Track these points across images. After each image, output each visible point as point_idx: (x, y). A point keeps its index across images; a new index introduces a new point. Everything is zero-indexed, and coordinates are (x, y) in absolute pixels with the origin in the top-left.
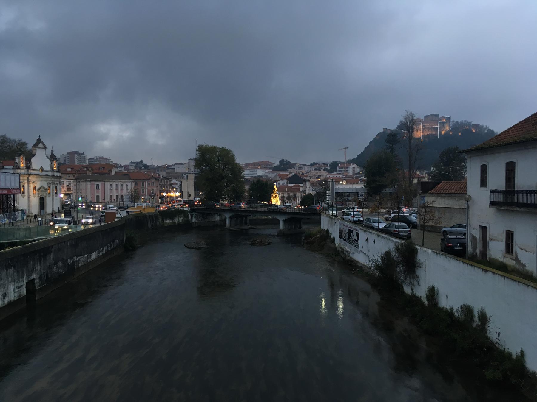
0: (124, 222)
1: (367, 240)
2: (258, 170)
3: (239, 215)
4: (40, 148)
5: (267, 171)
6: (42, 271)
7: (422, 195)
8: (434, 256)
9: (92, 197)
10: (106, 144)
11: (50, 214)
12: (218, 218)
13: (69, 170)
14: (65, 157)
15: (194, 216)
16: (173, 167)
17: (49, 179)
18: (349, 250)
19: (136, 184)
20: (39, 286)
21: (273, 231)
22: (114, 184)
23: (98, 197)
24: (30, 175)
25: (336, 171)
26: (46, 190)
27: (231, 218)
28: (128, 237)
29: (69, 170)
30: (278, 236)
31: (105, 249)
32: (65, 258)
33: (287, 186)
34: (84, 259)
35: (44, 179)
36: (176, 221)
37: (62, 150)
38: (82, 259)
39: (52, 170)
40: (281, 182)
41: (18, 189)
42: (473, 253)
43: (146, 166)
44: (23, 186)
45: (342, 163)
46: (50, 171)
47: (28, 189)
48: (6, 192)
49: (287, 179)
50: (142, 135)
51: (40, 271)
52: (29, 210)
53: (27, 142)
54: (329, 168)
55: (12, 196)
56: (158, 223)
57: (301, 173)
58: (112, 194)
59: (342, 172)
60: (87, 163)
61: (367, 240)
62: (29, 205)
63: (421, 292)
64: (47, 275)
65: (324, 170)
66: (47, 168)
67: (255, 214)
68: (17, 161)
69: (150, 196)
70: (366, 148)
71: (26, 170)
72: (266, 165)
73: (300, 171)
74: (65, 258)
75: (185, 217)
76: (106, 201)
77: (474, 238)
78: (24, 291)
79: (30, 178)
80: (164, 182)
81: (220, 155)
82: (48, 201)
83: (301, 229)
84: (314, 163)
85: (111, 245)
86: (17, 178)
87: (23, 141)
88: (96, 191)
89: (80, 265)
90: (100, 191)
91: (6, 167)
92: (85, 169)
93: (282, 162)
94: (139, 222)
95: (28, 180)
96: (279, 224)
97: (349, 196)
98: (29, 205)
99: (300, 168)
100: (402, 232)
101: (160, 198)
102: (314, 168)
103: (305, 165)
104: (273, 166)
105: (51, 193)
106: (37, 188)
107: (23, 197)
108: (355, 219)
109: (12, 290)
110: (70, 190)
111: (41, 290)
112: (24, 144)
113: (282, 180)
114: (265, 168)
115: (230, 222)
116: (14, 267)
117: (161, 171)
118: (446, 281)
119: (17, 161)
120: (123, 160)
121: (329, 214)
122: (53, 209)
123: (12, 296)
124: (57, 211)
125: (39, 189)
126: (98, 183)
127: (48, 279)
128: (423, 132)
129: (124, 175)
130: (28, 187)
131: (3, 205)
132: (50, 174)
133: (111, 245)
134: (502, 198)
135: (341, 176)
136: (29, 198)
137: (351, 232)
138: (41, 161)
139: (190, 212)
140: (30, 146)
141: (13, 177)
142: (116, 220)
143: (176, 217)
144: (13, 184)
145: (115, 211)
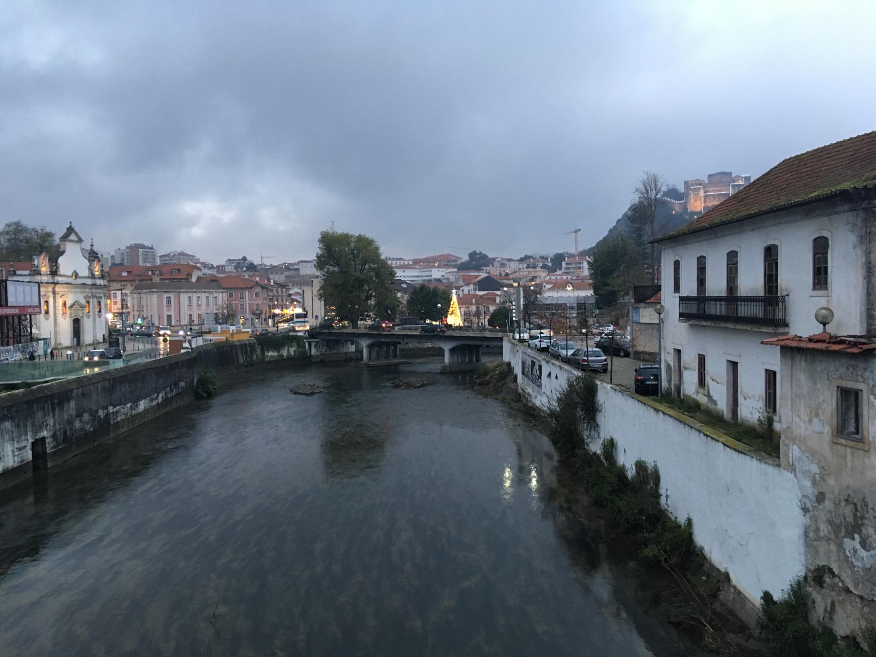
0: (193, 355)
1: (549, 375)
2: (433, 270)
3: (383, 343)
4: (71, 241)
5: (449, 270)
6: (58, 427)
7: (636, 305)
8: (612, 394)
9: (160, 318)
10: (197, 231)
11: (90, 345)
12: (352, 348)
13: (125, 274)
14: (123, 254)
15: (313, 345)
16: (296, 267)
17: (88, 290)
18: (531, 393)
19: (231, 295)
20: (53, 448)
21: (435, 366)
22: (194, 297)
23: (169, 317)
24: (56, 283)
25: (561, 269)
26: (82, 307)
27: (370, 347)
28: (208, 377)
29: (125, 274)
30: (441, 373)
31: (161, 395)
32: (94, 408)
33: (475, 296)
34: (125, 410)
35: (79, 290)
36: (284, 352)
37: (111, 242)
38: (122, 410)
39: (93, 276)
40: (466, 289)
41: (36, 307)
42: (668, 389)
43: (252, 267)
44: (47, 302)
45: (571, 256)
46: (88, 277)
47: (55, 306)
48: (17, 311)
49: (475, 284)
50: (247, 216)
51: (54, 425)
52: (56, 339)
53: (53, 232)
54: (550, 264)
55: (28, 317)
56: (255, 357)
57: (503, 274)
58: (191, 313)
59: (571, 270)
60: (158, 262)
61: (549, 375)
62: (56, 333)
63: (596, 447)
64: (65, 433)
65: (542, 267)
66: (84, 272)
67: (406, 341)
68: (36, 263)
69: (254, 314)
70: (611, 231)
71: (50, 277)
72: (446, 261)
73: (502, 269)
74: (94, 408)
75: (299, 346)
76: (182, 323)
77: (669, 367)
78: (28, 455)
79: (57, 289)
80: (277, 291)
81: (355, 248)
82: (87, 325)
83: (474, 365)
84: (526, 256)
85: (171, 390)
86: (36, 289)
87: (48, 230)
88: (165, 307)
89: (119, 419)
90: (173, 308)
91: (18, 272)
92: (150, 273)
93: (473, 255)
94: (223, 355)
95: (54, 293)
96: (444, 355)
97: (548, 309)
98: (56, 333)
99: (503, 265)
100: (594, 361)
101: (270, 317)
102: (525, 265)
103: (510, 260)
104: (459, 262)
105: (91, 313)
106: (68, 305)
107: (47, 319)
108: (544, 345)
109: (10, 454)
110: (127, 308)
111: (54, 454)
112: (50, 235)
113: (468, 284)
114: (446, 266)
115: (370, 353)
116: (13, 419)
117: (277, 273)
118: (630, 430)
119: (36, 263)
120: (215, 257)
121: (514, 338)
122: (95, 336)
123: (10, 461)
124: (101, 340)
125: (71, 307)
126: (168, 295)
127: (67, 440)
128: (705, 201)
129: (213, 282)
130: (55, 303)
131: (14, 331)
132: (89, 282)
133: (171, 390)
134: (693, 309)
135: (570, 277)
136: (55, 320)
137: (533, 363)
138: (72, 261)
139: (306, 338)
140: (57, 239)
141: (27, 288)
142: (183, 351)
143: (284, 346)
144: (28, 300)
145: (181, 338)
